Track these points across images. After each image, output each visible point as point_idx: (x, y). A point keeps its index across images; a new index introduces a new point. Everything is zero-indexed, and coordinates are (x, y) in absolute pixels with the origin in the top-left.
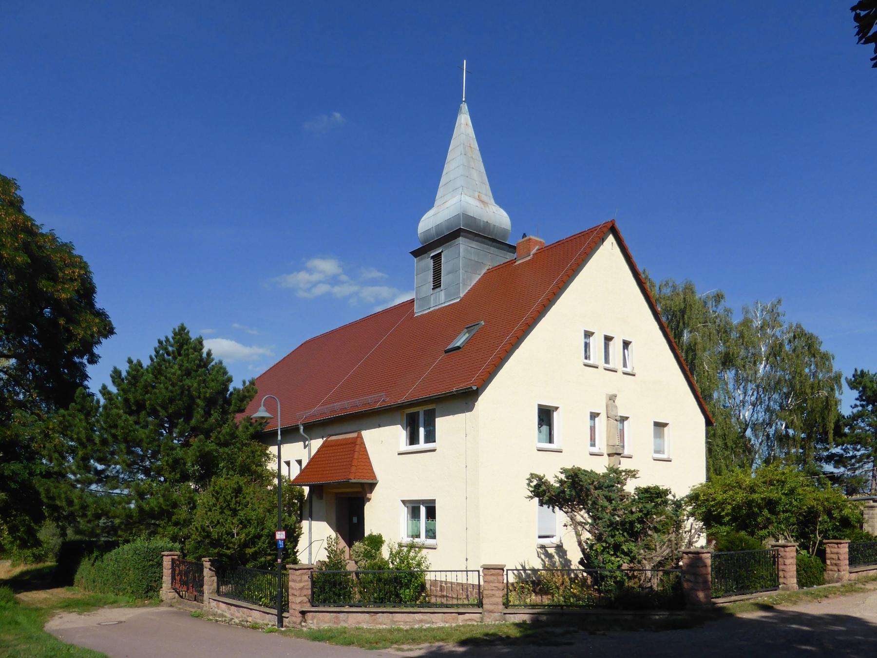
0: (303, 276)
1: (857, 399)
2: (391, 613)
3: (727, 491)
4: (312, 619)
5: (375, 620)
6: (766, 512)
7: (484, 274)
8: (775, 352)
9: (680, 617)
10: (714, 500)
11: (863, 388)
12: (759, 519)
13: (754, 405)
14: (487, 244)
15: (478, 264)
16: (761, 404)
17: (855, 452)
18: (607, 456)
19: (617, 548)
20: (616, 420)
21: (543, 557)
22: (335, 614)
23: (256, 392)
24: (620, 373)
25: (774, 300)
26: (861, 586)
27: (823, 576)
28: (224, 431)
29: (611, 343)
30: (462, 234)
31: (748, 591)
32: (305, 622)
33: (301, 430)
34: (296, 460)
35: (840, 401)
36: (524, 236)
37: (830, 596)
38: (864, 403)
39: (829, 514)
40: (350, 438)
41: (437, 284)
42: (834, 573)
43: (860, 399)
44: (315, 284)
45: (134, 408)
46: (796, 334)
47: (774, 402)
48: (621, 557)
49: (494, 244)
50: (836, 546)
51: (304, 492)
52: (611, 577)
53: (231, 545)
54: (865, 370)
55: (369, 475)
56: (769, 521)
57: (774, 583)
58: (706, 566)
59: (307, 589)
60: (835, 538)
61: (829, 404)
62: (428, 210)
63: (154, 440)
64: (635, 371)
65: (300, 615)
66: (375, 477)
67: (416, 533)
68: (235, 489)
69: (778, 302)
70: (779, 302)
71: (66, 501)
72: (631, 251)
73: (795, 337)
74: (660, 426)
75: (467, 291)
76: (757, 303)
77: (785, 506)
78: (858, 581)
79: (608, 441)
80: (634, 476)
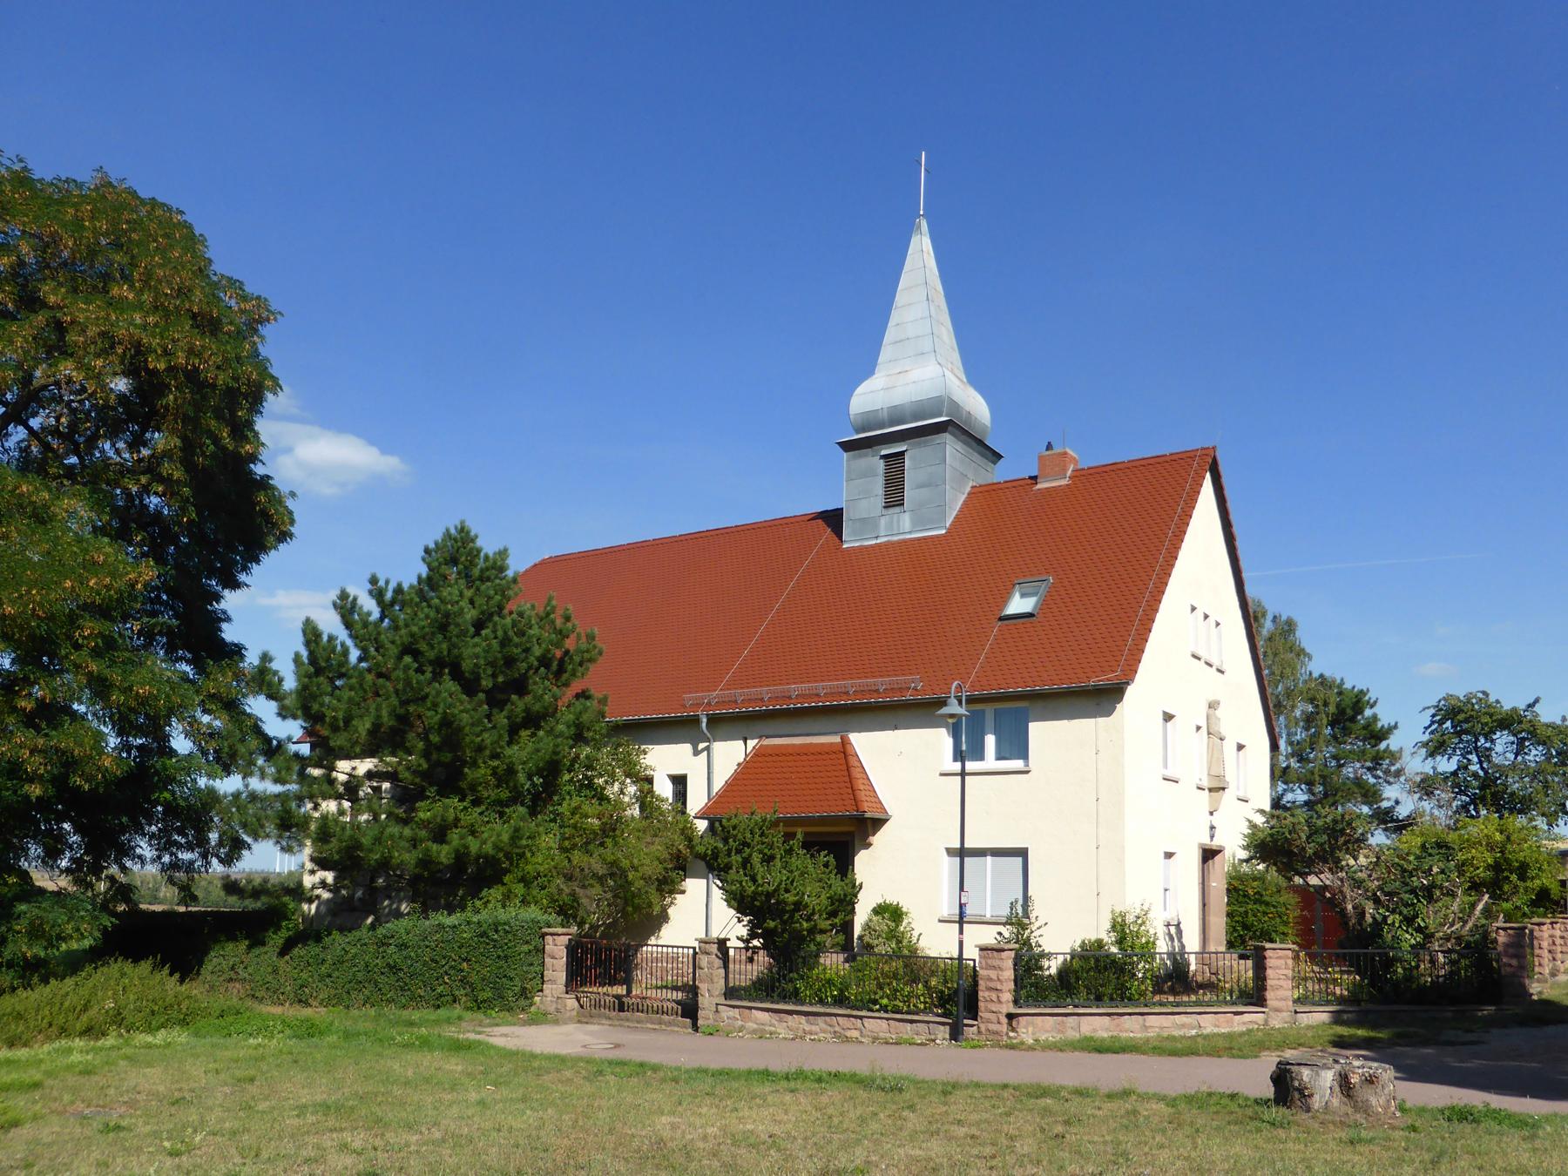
2: (1142, 1014)
6: (1514, 877)
22: (1060, 1018)
23: (600, 653)
30: (950, 428)
32: (1013, 1030)
33: (704, 725)
34: (669, 776)
36: (1049, 447)
79: (1209, 769)
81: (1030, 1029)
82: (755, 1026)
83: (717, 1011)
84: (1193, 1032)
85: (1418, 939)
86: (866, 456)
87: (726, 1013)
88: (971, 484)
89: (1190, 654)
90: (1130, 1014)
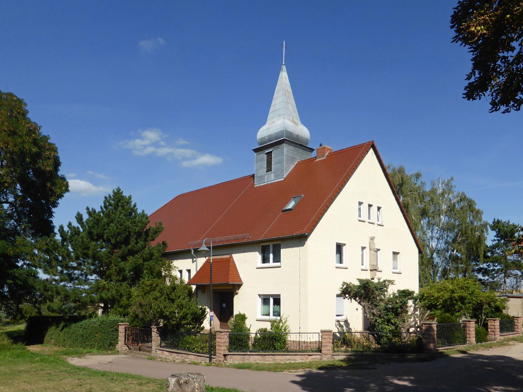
0: (138, 142)
1: (495, 236)
3: (439, 292)
4: (230, 359)
5: (264, 359)
6: (459, 303)
7: (296, 165)
8: (451, 209)
9: (422, 357)
10: (433, 296)
11: (498, 230)
12: (456, 307)
13: (438, 239)
14: (298, 147)
15: (292, 159)
16: (442, 239)
17: (494, 267)
18: (370, 271)
19: (389, 321)
20: (375, 251)
21: (338, 326)
22: (243, 356)
23: (163, 229)
24: (376, 225)
25: (450, 178)
26: (506, 342)
27: (487, 337)
28: (146, 252)
29: (371, 208)
31: (452, 345)
32: (226, 360)
33: (193, 252)
34: (186, 270)
35: (487, 237)
36: (321, 145)
37: (493, 347)
38: (499, 239)
39: (489, 305)
40: (225, 258)
41: (269, 169)
42: (492, 336)
43: (497, 236)
44: (145, 147)
45: (95, 238)
46: (462, 198)
47: (450, 238)
48: (390, 326)
49: (302, 147)
50: (493, 321)
51: (192, 288)
52: (385, 336)
53: (174, 319)
54: (500, 220)
55: (238, 280)
56: (461, 308)
57: (464, 341)
58: (434, 331)
59: (227, 343)
60: (491, 317)
61: (480, 240)
62: (262, 126)
63: (109, 257)
64: (383, 224)
65: (223, 357)
66: (241, 281)
67: (267, 313)
68: (172, 288)
69: (451, 179)
70: (452, 179)
71: (56, 292)
72: (382, 158)
73: (461, 200)
74: (395, 254)
75: (287, 174)
76: (439, 179)
77: (469, 300)
78: (504, 340)
79: (370, 262)
80: (392, 284)
81: (232, 360)
82: (165, 357)
83: (156, 351)
84: (293, 362)
85: (393, 328)
86: (261, 153)
87: (159, 352)
88: (298, 161)
89: (357, 220)
90: (269, 355)
